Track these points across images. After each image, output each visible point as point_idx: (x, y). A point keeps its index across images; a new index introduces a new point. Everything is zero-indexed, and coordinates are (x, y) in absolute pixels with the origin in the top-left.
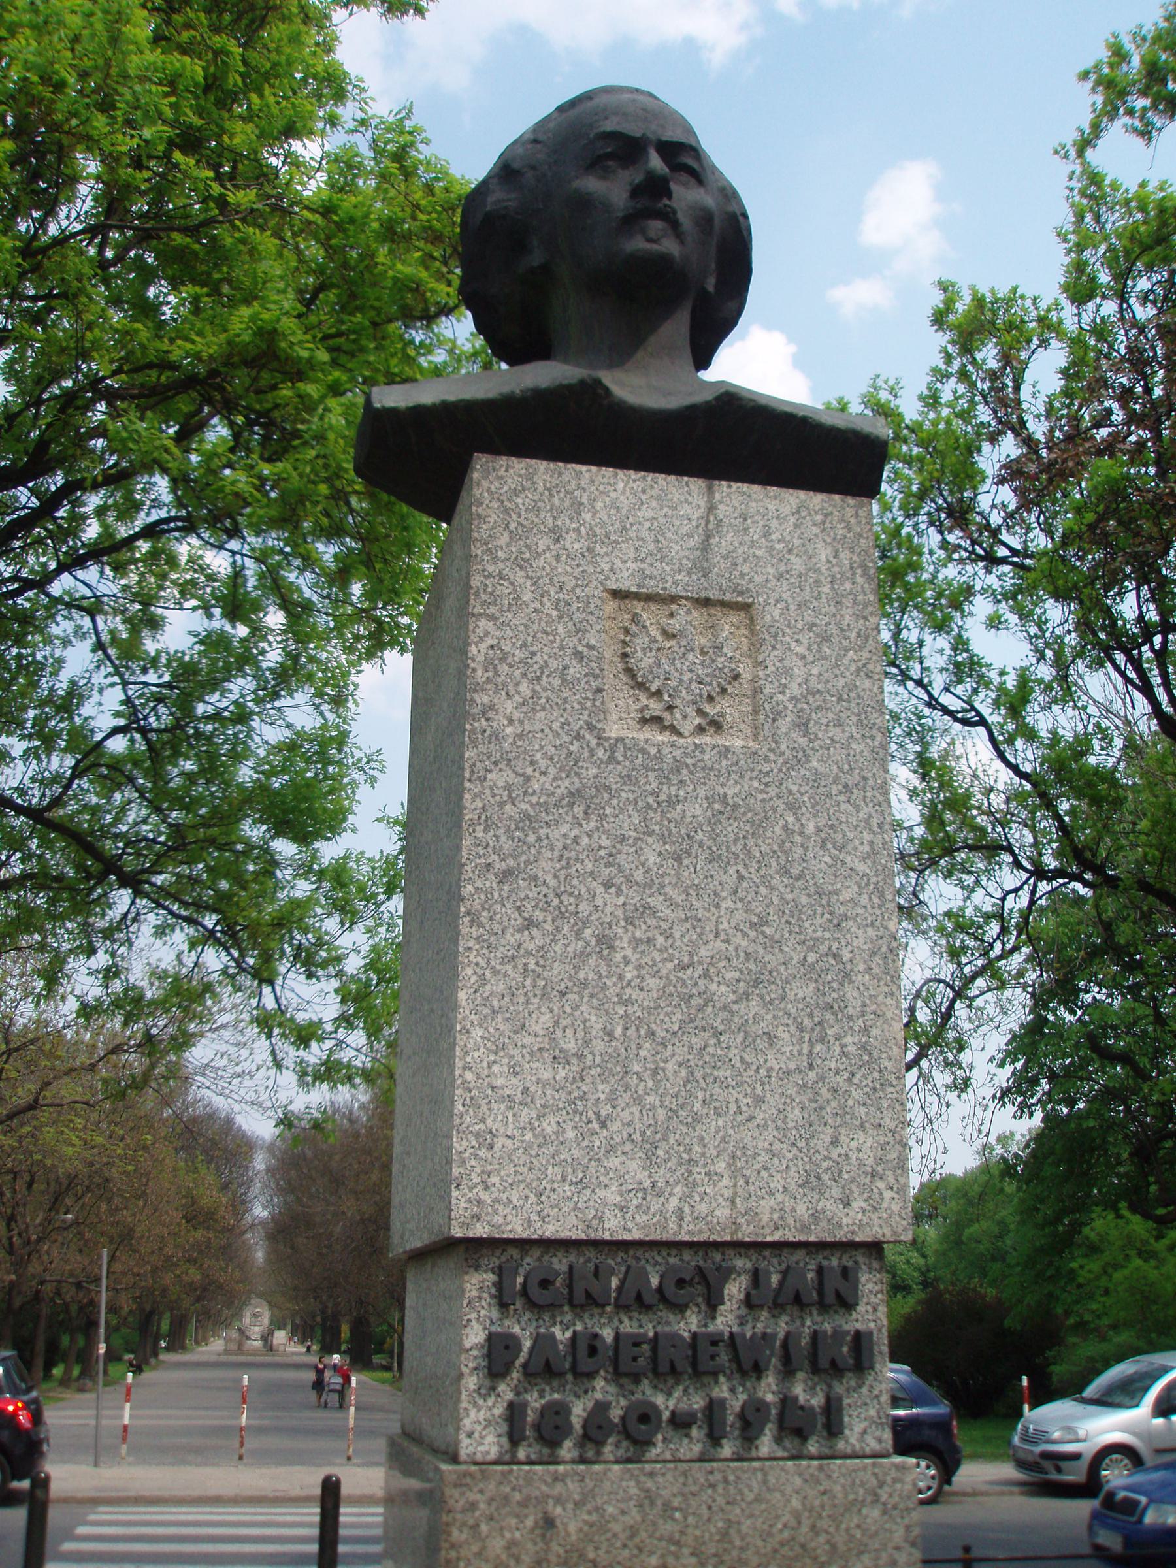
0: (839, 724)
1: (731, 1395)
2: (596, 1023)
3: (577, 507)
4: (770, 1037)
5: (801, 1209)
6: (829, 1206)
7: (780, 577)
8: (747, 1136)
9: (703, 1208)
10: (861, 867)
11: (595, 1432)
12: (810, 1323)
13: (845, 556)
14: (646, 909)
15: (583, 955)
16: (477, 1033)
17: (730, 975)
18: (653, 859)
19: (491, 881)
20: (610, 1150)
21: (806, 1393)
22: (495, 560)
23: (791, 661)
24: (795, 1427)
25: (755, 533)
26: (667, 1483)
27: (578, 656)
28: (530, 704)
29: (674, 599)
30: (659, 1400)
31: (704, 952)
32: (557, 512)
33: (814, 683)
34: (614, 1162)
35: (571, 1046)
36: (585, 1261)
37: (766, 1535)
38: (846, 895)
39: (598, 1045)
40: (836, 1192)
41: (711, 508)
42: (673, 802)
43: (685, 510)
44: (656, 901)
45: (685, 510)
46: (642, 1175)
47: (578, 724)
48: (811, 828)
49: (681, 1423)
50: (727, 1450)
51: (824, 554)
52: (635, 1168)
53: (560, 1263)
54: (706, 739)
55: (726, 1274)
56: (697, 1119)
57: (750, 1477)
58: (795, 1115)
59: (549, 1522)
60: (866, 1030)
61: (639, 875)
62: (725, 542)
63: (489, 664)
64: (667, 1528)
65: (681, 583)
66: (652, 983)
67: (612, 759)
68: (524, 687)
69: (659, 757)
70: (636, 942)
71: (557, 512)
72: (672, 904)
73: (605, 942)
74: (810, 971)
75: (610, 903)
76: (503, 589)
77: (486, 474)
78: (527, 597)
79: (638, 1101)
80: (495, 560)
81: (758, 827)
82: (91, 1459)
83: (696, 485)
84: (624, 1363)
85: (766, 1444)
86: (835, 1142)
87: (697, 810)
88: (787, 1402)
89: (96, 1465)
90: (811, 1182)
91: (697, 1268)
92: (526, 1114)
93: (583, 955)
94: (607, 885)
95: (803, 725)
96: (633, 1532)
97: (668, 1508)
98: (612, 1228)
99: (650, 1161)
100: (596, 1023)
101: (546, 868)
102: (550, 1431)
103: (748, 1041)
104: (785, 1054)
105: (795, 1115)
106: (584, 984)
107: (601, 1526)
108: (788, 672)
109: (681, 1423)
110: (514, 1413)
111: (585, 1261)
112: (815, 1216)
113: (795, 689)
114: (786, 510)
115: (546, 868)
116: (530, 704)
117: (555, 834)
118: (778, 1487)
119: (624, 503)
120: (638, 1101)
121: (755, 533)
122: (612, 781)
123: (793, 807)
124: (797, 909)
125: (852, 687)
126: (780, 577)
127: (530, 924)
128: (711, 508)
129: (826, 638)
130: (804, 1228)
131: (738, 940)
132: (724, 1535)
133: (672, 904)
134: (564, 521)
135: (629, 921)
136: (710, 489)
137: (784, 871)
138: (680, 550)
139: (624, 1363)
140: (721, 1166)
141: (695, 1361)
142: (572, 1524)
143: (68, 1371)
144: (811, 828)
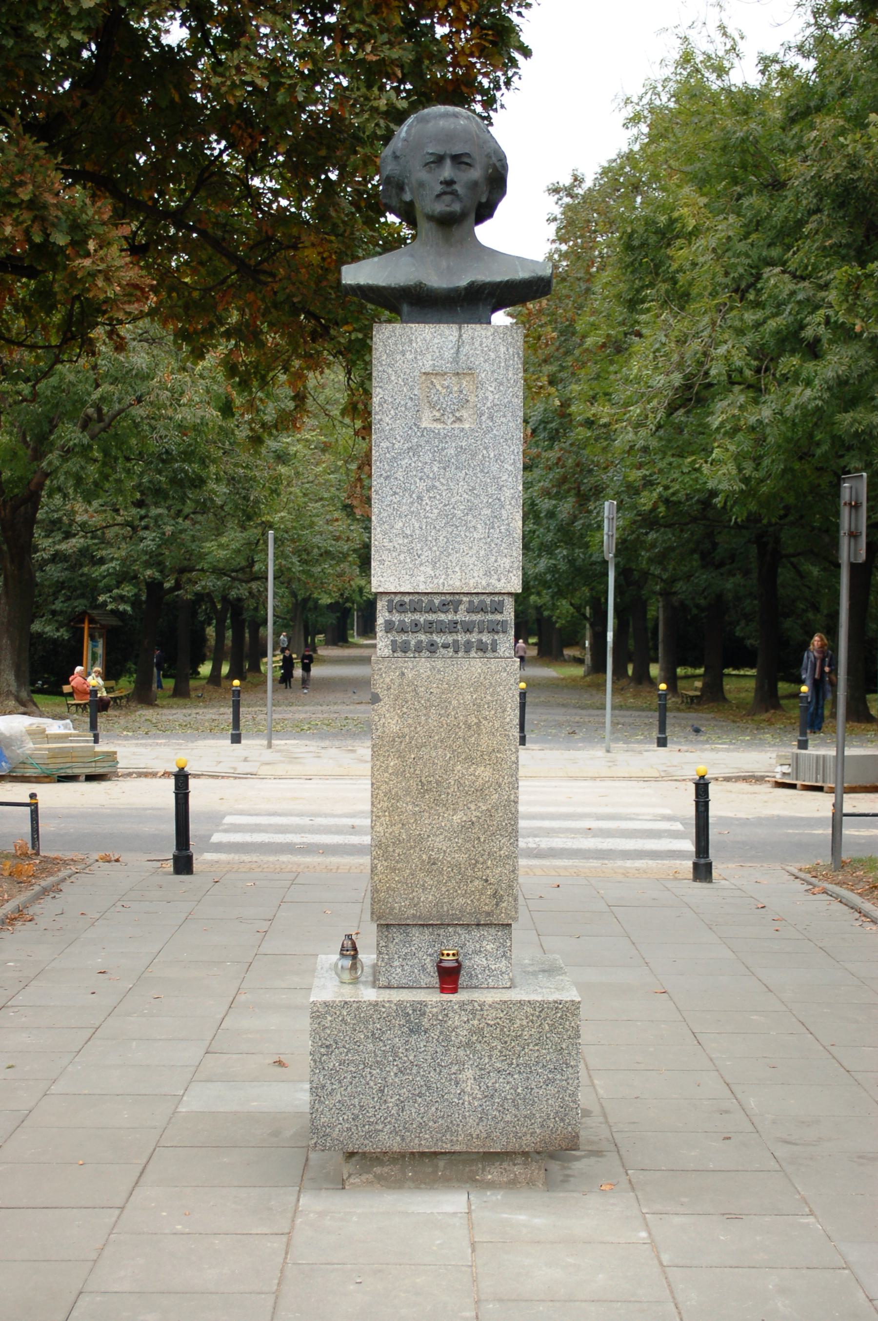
0: (504, 416)
1: (461, 638)
2: (417, 525)
3: (411, 341)
4: (475, 528)
5: (484, 583)
6: (493, 581)
7: (485, 361)
8: (466, 559)
9: (451, 582)
10: (510, 468)
11: (419, 649)
12: (490, 617)
13: (511, 350)
14: (434, 487)
15: (412, 503)
16: (379, 529)
17: (462, 507)
18: (436, 469)
19: (382, 480)
20: (421, 564)
21: (486, 638)
22: (382, 365)
23: (488, 394)
24: (482, 648)
25: (477, 344)
26: (439, 664)
27: (411, 399)
28: (395, 418)
29: (445, 374)
30: (438, 640)
31: (453, 500)
32: (403, 344)
33: (496, 401)
34: (422, 568)
35: (408, 532)
36: (416, 598)
37: (469, 680)
38: (504, 478)
39: (417, 532)
40: (496, 577)
41: (460, 336)
42: (443, 449)
43: (451, 338)
44: (437, 484)
45: (451, 338)
46: (432, 573)
47: (411, 423)
48: (492, 455)
49: (445, 646)
50: (460, 654)
51: (503, 349)
52: (429, 570)
53: (407, 599)
54: (456, 425)
55: (460, 602)
56: (450, 554)
57: (466, 663)
58: (482, 553)
59: (403, 674)
60: (508, 525)
61: (431, 475)
62: (465, 350)
63: (380, 404)
64: (438, 676)
65: (448, 367)
66: (436, 511)
67: (422, 435)
68: (392, 412)
69: (439, 434)
70: (430, 498)
71: (403, 344)
72: (443, 484)
73: (420, 498)
74: (489, 505)
75: (422, 485)
76: (385, 376)
77: (378, 332)
78: (393, 378)
79: (430, 549)
80: (382, 365)
81: (473, 456)
82: (655, 734)
83: (455, 327)
84: (430, 628)
85: (473, 654)
86: (496, 561)
87: (452, 451)
88: (480, 641)
89: (662, 743)
90: (488, 574)
91: (450, 601)
92: (394, 554)
93: (412, 503)
94: (420, 479)
95: (491, 418)
96: (428, 677)
97: (439, 670)
98: (422, 588)
99: (434, 568)
100: (417, 525)
101: (400, 474)
102: (405, 648)
103: (468, 529)
104: (481, 531)
105: (482, 553)
106: (413, 512)
107: (419, 675)
108: (487, 398)
109: (445, 646)
110: (394, 642)
111: (416, 598)
112: (488, 585)
113: (489, 404)
114: (489, 334)
115: (400, 474)
116: (395, 418)
117: (403, 463)
118: (475, 666)
119: (428, 338)
120: (430, 549)
121: (477, 344)
122: (422, 443)
123: (486, 448)
124: (486, 485)
125: (510, 402)
126: (485, 361)
127: (395, 493)
128: (460, 336)
129: (501, 384)
130: (484, 588)
131: (465, 496)
132: (457, 679)
133: (443, 484)
134: (406, 347)
135: (428, 491)
136: (460, 328)
137: (482, 471)
138: (448, 354)
139: (430, 628)
140: (457, 569)
141: (453, 627)
142: (410, 675)
143: (216, 669)
144: (492, 455)
